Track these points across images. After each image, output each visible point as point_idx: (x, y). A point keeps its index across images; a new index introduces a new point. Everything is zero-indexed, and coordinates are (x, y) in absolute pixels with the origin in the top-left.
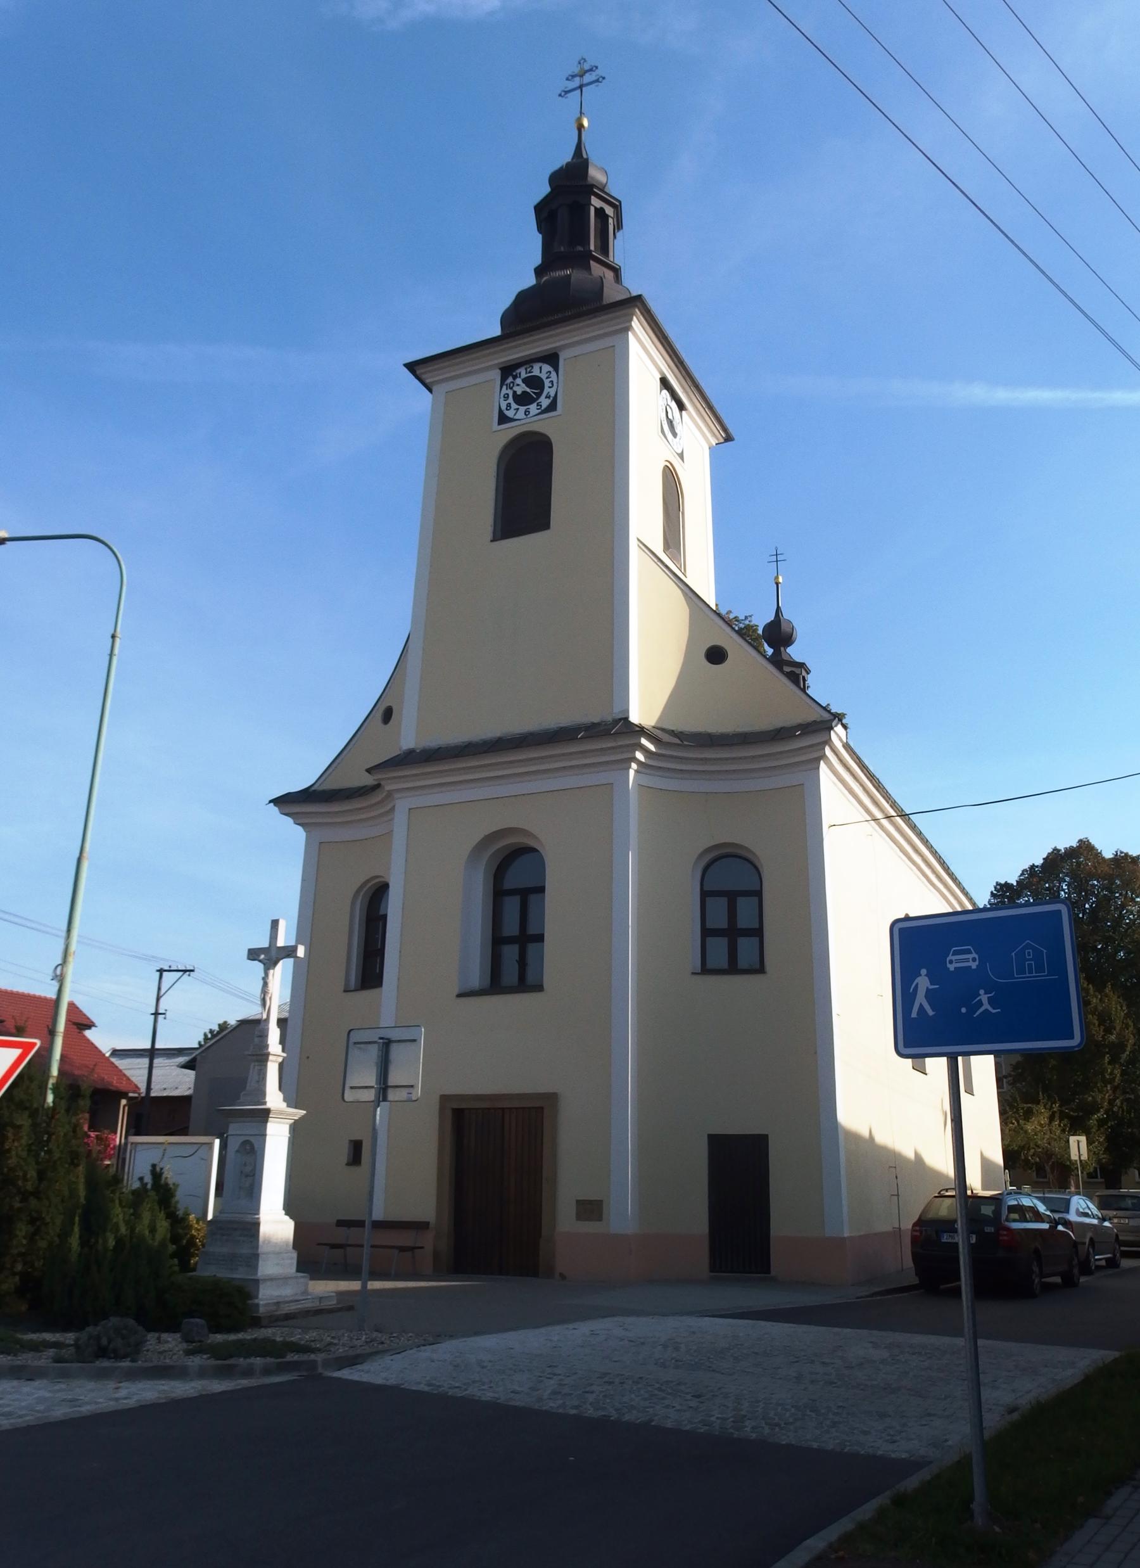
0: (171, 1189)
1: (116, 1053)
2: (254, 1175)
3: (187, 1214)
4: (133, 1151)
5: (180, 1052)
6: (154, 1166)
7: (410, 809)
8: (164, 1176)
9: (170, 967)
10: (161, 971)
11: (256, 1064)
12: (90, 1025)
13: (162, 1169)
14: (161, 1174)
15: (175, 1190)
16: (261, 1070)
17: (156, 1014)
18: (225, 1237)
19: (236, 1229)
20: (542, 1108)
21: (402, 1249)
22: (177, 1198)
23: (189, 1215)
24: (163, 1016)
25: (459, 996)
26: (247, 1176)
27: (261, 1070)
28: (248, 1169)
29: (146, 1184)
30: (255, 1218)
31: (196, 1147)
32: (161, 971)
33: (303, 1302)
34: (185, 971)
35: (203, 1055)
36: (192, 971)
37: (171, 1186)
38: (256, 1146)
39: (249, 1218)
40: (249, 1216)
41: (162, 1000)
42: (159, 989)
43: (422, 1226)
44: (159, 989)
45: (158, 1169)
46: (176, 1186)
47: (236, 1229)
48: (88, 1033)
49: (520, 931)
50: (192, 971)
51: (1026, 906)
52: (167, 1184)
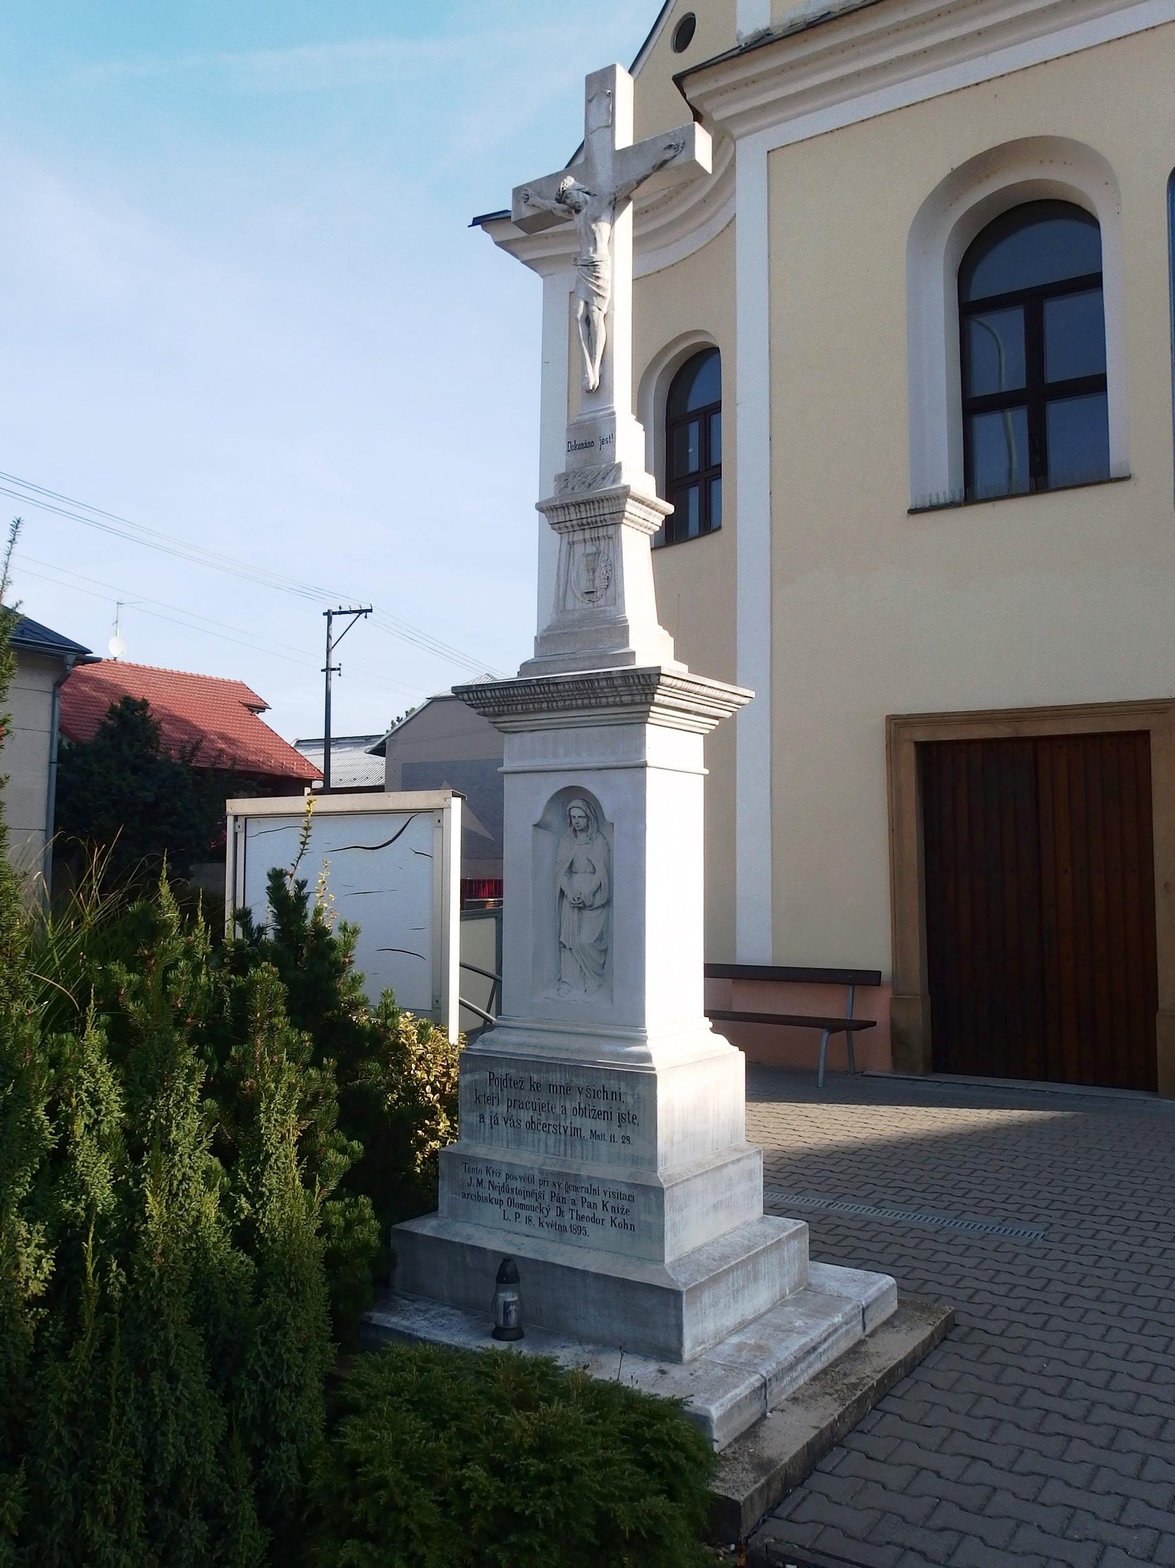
0: (332, 945)
1: (299, 743)
2: (608, 903)
3: (389, 1013)
4: (241, 837)
5: (368, 739)
6: (277, 877)
7: (768, 152)
8: (310, 907)
9: (340, 608)
10: (329, 614)
11: (578, 536)
12: (262, 708)
13: (301, 885)
14: (302, 900)
15: (348, 946)
16: (597, 554)
17: (328, 670)
18: (525, 1116)
19: (566, 1090)
20: (1145, 735)
21: (833, 1026)
22: (355, 970)
23: (393, 1015)
24: (338, 671)
25: (912, 512)
26: (581, 907)
27: (597, 554)
28: (582, 885)
29: (261, 930)
30: (630, 1056)
31: (398, 822)
32: (329, 614)
33: (825, 1346)
34: (360, 612)
35: (393, 738)
36: (371, 611)
37: (336, 935)
38: (608, 809)
39: (606, 1055)
40: (607, 1047)
41: (333, 653)
42: (329, 636)
43: (867, 979)
44: (329, 636)
45: (290, 887)
46: (350, 932)
47: (566, 1090)
48: (261, 716)
49: (1029, 379)
50: (371, 611)
51: (222, 908)
52: (321, 932)
